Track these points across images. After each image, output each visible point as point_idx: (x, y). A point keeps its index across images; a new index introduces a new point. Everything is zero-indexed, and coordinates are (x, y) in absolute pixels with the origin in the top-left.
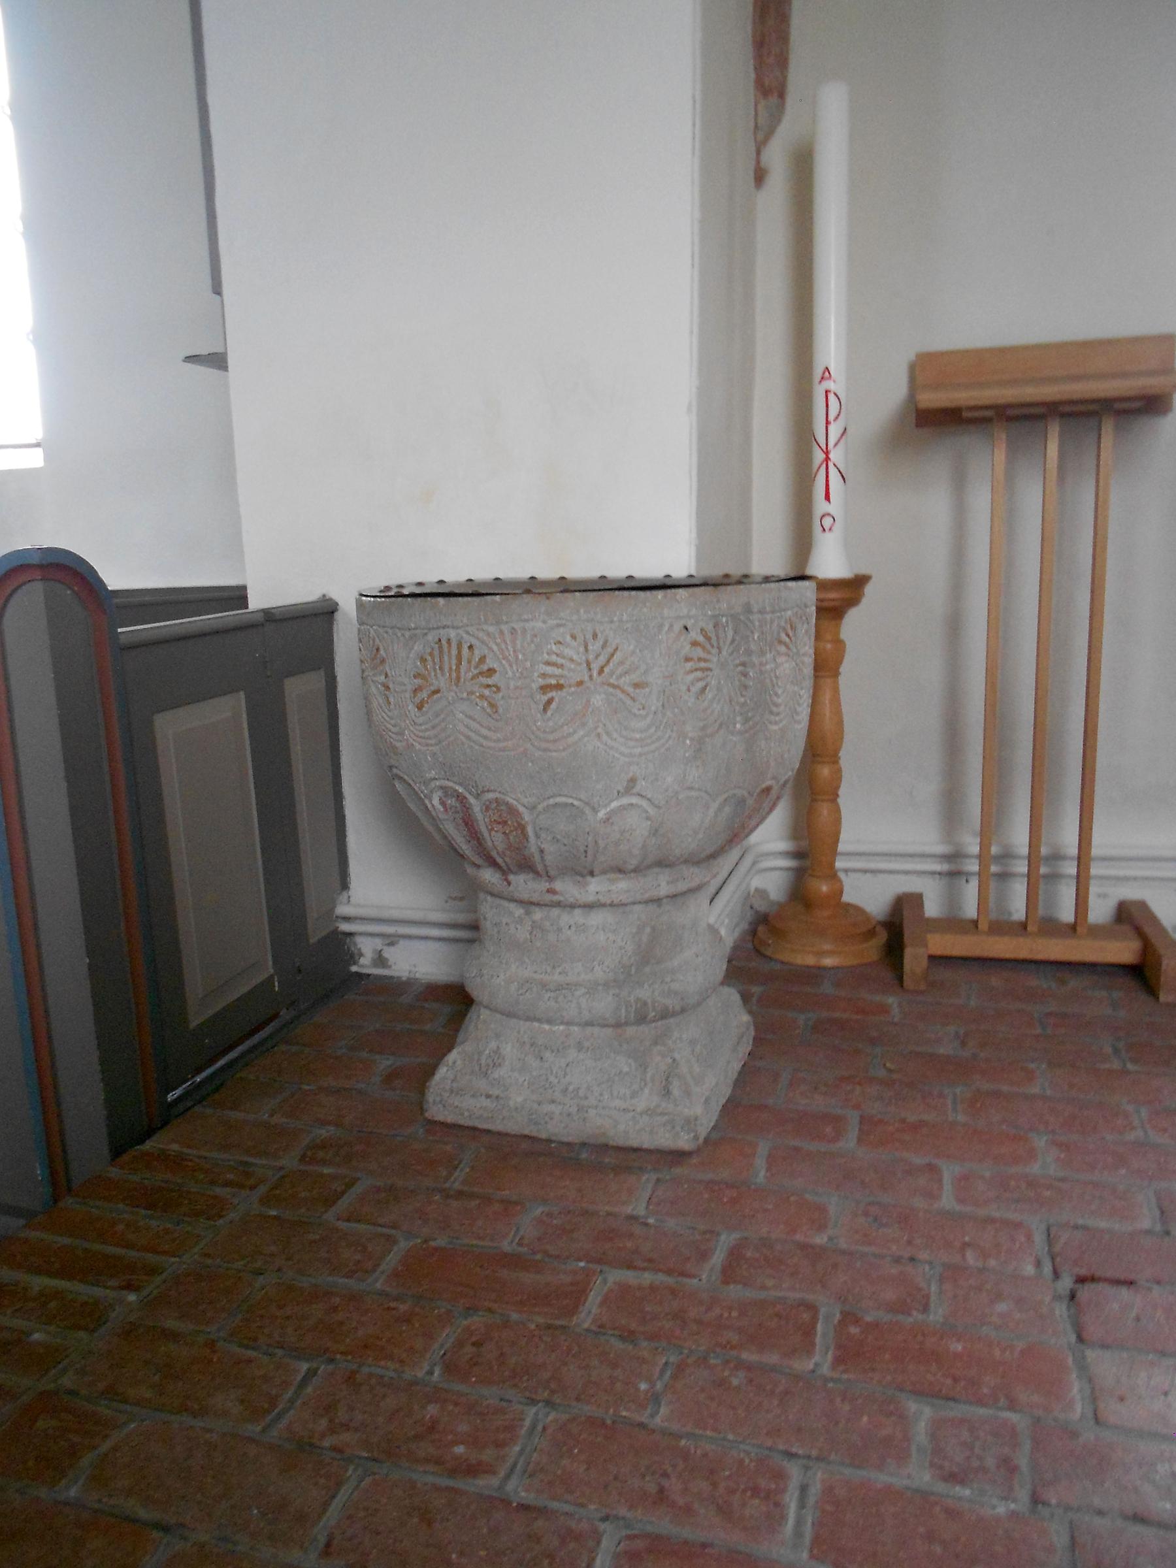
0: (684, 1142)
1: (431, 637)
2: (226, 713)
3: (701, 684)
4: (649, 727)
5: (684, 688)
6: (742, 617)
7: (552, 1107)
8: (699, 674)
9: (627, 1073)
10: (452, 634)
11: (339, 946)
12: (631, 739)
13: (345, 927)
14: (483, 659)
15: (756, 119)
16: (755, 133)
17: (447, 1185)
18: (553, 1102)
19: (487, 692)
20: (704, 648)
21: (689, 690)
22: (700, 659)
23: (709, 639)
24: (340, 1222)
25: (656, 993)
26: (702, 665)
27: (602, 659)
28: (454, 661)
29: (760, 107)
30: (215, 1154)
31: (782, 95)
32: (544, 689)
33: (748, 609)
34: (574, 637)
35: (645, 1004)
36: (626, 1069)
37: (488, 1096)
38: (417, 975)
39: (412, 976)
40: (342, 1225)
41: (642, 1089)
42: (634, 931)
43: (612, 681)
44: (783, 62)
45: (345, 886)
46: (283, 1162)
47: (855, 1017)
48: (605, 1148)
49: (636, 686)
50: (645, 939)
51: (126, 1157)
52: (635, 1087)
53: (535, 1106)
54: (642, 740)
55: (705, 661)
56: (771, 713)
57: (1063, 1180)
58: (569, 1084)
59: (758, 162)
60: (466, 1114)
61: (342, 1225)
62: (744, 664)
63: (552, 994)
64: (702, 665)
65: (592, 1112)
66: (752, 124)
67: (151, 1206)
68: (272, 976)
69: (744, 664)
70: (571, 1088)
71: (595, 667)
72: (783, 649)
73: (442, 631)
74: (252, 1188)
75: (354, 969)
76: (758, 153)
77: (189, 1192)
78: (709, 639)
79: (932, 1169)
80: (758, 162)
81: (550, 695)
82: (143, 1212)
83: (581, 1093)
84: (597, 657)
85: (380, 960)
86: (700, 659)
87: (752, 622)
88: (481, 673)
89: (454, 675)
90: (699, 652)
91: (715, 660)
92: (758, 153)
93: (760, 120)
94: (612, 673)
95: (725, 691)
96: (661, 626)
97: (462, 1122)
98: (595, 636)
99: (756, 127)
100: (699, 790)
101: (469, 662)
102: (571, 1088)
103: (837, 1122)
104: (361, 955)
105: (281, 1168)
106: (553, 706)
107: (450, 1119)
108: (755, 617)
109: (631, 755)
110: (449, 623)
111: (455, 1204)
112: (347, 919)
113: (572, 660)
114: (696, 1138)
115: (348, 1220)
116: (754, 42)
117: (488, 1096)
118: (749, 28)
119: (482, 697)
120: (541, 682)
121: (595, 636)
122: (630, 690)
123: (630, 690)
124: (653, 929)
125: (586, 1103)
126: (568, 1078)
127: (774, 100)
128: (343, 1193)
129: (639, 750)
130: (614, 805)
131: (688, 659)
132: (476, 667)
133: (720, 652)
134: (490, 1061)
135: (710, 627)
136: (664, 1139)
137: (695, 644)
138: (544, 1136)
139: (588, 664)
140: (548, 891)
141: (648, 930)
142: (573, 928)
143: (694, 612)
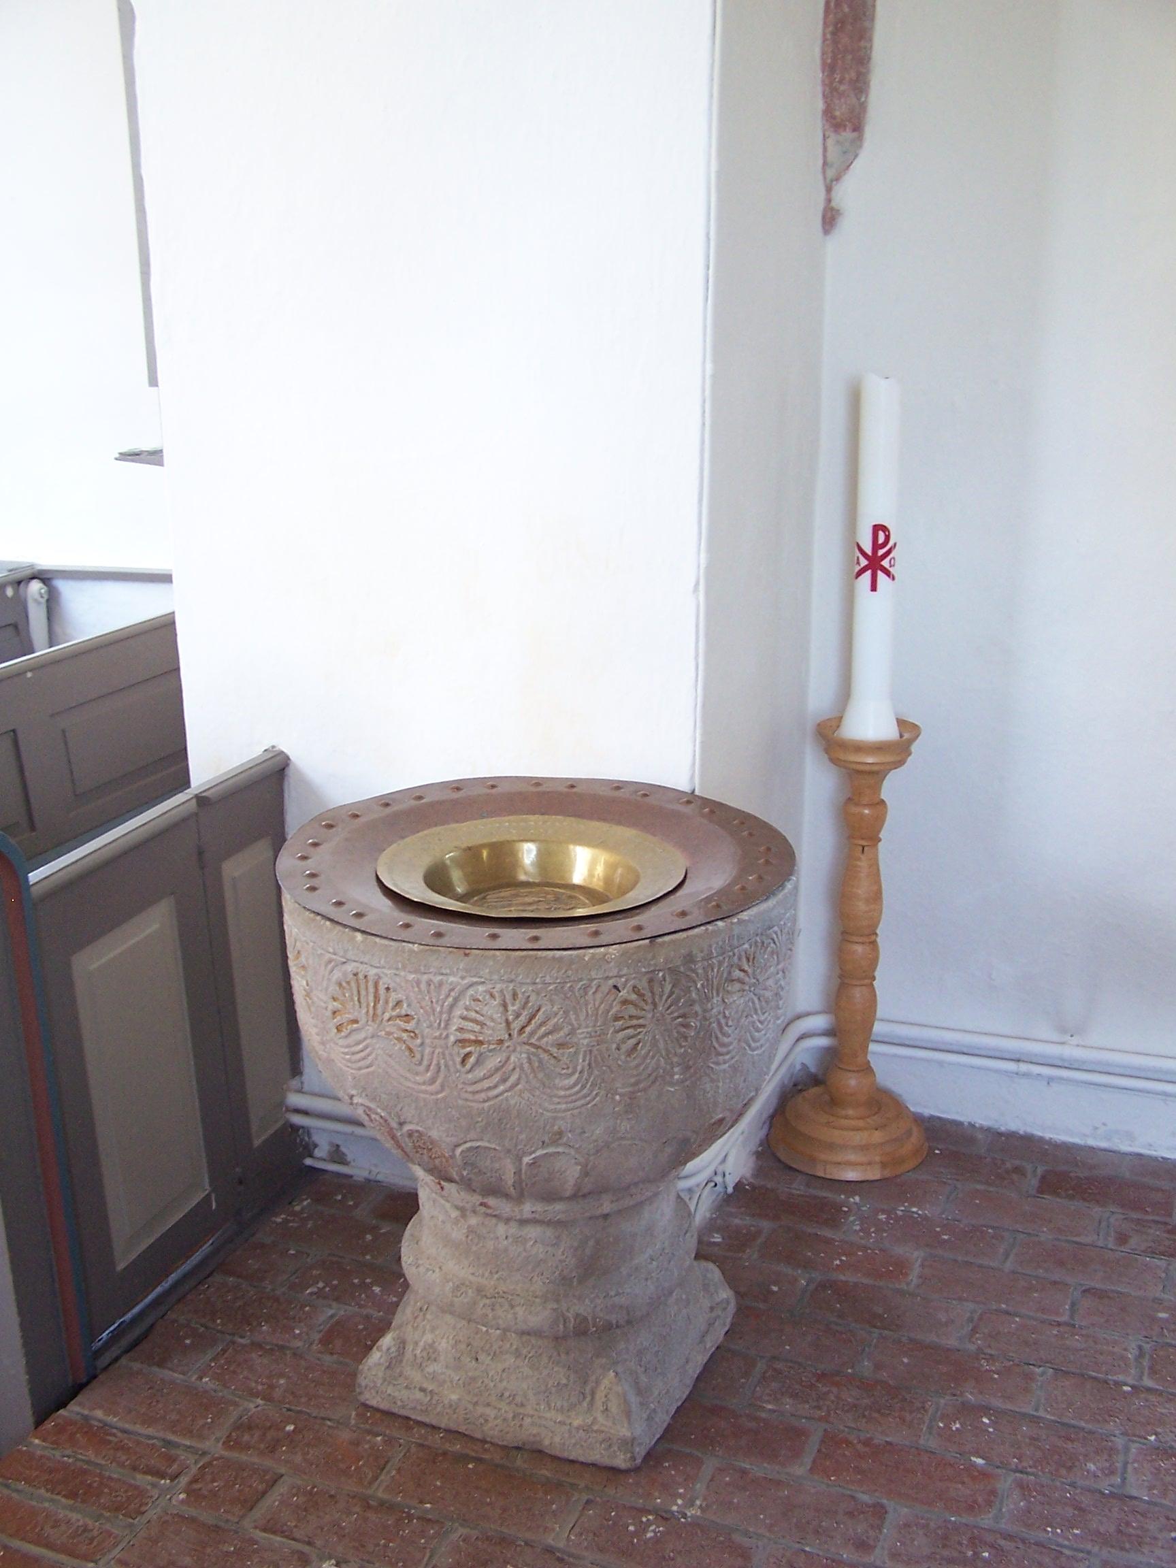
0: (621, 1461)
1: (350, 967)
2: (153, 927)
3: (633, 1041)
4: (575, 1085)
5: (614, 1046)
6: (682, 969)
7: (488, 1411)
8: (630, 1031)
9: (566, 1385)
10: (372, 972)
11: (293, 1141)
12: (556, 1096)
13: (297, 1119)
14: (398, 1003)
15: (825, 156)
16: (824, 172)
17: (370, 1492)
18: (488, 1405)
19: (405, 1036)
20: (636, 1005)
21: (618, 1049)
22: (631, 1017)
23: (641, 995)
24: (257, 1531)
25: (598, 1309)
26: (635, 1022)
27: (523, 1019)
28: (371, 998)
29: (830, 142)
30: (138, 1428)
31: (858, 128)
32: (462, 1042)
33: (689, 959)
34: (492, 996)
35: (585, 1319)
36: (564, 1381)
37: (422, 1390)
38: (379, 1178)
39: (372, 1177)
40: (258, 1535)
41: (580, 1403)
42: (576, 1244)
43: (533, 1041)
44: (860, 85)
45: (296, 1069)
46: (207, 1445)
47: (866, 1281)
48: (538, 1453)
49: (560, 1045)
50: (588, 1252)
51: (50, 1425)
52: (573, 1400)
53: (470, 1407)
54: (565, 1097)
55: (639, 1018)
56: (719, 1054)
57: (1009, 1537)
58: (505, 1389)
59: (829, 200)
60: (399, 1403)
61: (258, 1535)
62: (683, 1016)
63: (488, 1301)
64: (635, 1022)
65: (528, 1421)
66: (820, 162)
67: (72, 1495)
68: (209, 1195)
69: (683, 1016)
70: (507, 1394)
71: (516, 1026)
72: (737, 986)
73: (362, 967)
74: (173, 1478)
75: (308, 1162)
76: (829, 189)
77: (110, 1478)
78: (641, 995)
79: (879, 1512)
80: (829, 200)
81: (468, 1049)
82: (63, 1500)
83: (519, 1399)
84: (518, 1016)
85: (337, 1155)
86: (631, 1017)
87: (694, 971)
88: (399, 1016)
89: (371, 1012)
90: (632, 1010)
91: (650, 1015)
92: (829, 189)
93: (831, 156)
94: (532, 1033)
95: (661, 1045)
96: (585, 989)
97: (395, 1410)
98: (515, 996)
99: (825, 164)
100: (633, 1139)
101: (387, 1002)
102: (507, 1394)
103: (797, 1435)
104: (316, 1146)
105: (204, 1453)
106: (472, 1060)
107: (384, 1406)
108: (699, 967)
109: (555, 1111)
110: (366, 960)
111: (372, 1516)
112: (298, 1111)
113: (492, 1020)
114: (633, 1458)
115: (265, 1530)
116: (824, 64)
117: (422, 1390)
118: (817, 51)
119: (399, 1039)
120: (460, 1036)
121: (515, 996)
122: (554, 1050)
123: (554, 1050)
124: (597, 1242)
125: (521, 1410)
126: (505, 1383)
127: (848, 135)
128: (264, 1493)
129: (564, 1106)
130: (538, 1153)
131: (617, 1019)
132: (393, 1009)
133: (655, 1005)
134: (425, 1354)
135: (643, 984)
136: (597, 1455)
137: (625, 1002)
138: (479, 1436)
139: (508, 1023)
140: (481, 1204)
141: (591, 1243)
142: (510, 1240)
143: (625, 971)
